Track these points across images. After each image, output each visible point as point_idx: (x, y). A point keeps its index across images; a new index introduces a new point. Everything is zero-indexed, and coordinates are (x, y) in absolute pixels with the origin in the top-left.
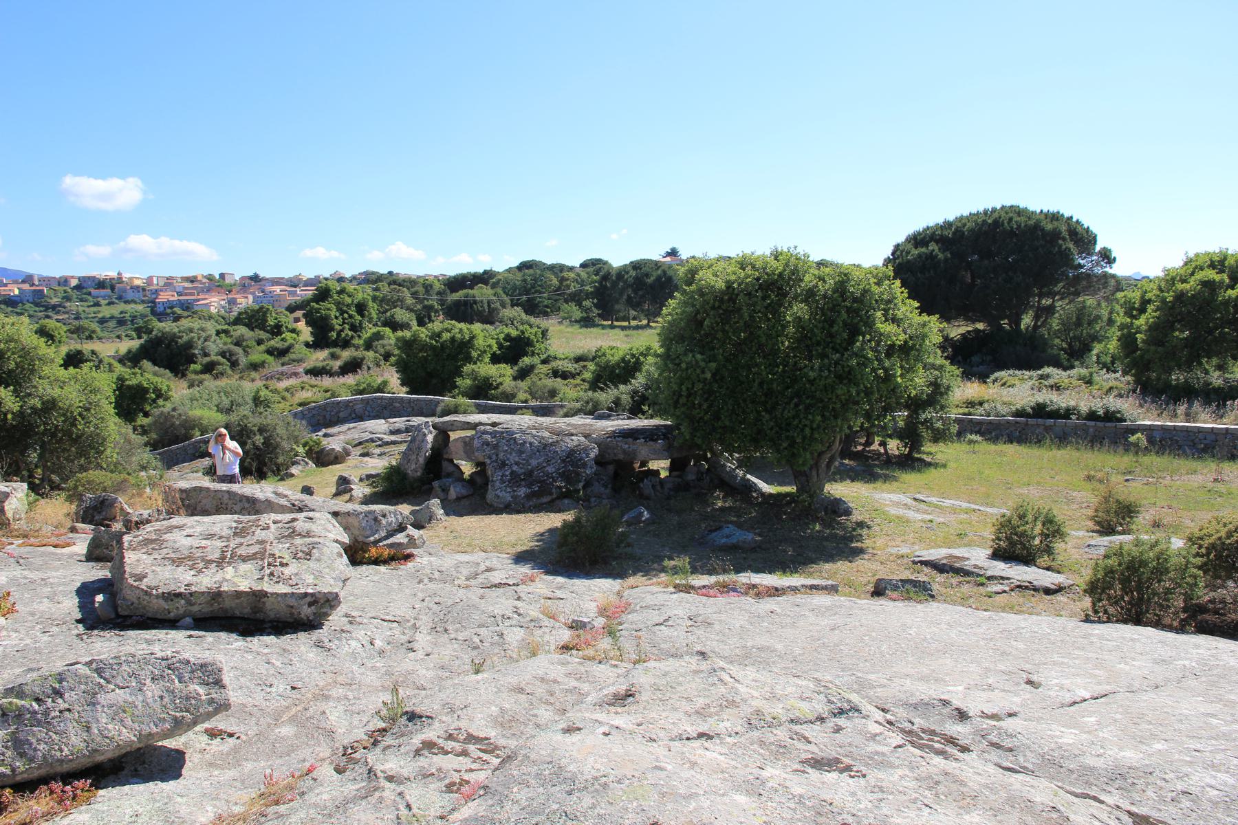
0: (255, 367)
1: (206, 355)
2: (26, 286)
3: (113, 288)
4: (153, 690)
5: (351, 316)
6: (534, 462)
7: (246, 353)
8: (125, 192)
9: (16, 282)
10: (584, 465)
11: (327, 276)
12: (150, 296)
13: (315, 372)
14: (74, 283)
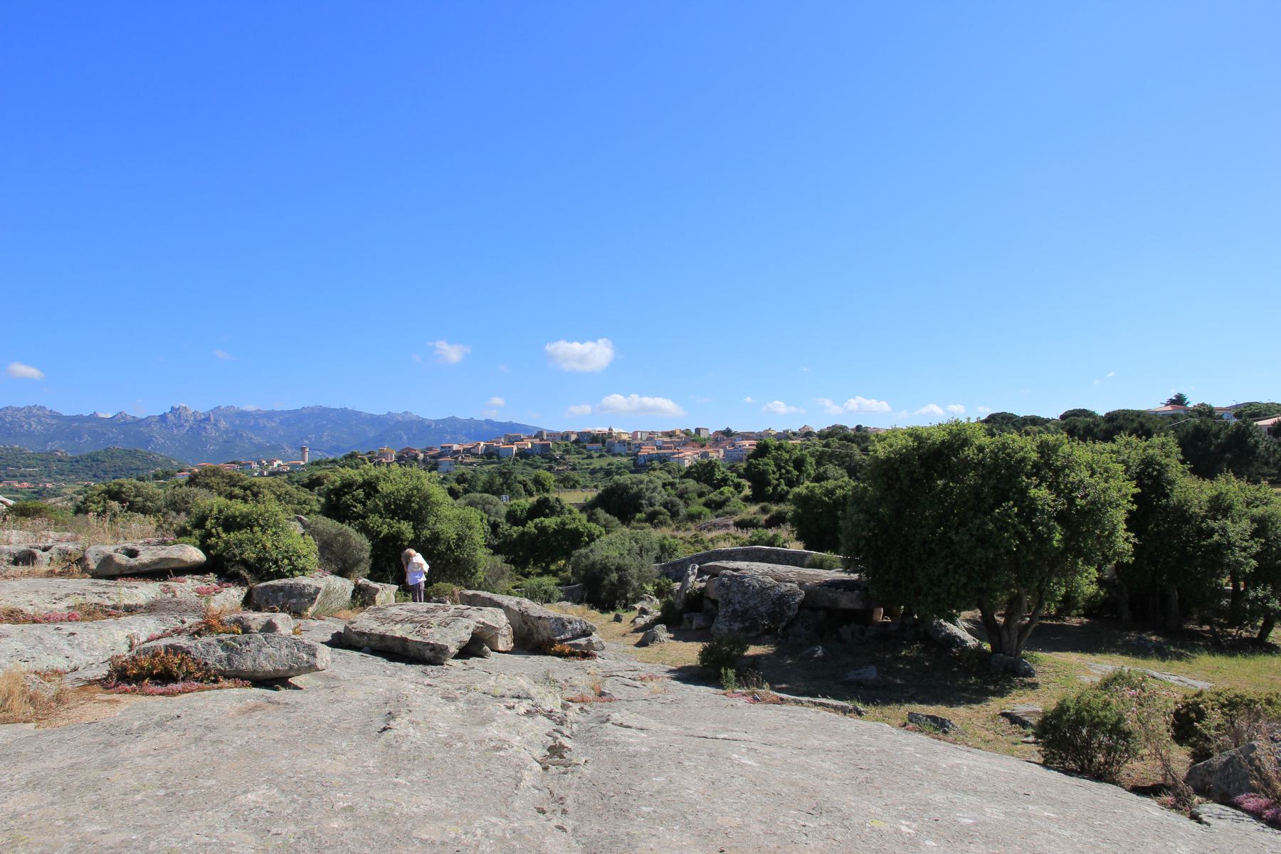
0: (692, 517)
1: (652, 505)
2: (537, 441)
3: (603, 442)
4: (285, 651)
5: (788, 472)
6: (751, 603)
7: (687, 504)
8: (598, 353)
9: (530, 437)
10: (789, 608)
11: (796, 430)
12: (634, 450)
13: (742, 525)
14: (573, 437)
